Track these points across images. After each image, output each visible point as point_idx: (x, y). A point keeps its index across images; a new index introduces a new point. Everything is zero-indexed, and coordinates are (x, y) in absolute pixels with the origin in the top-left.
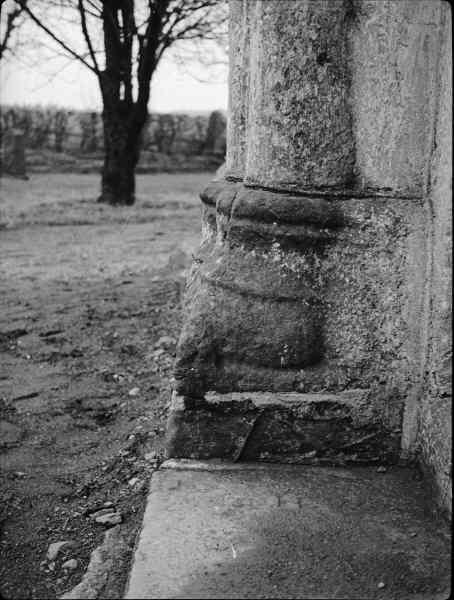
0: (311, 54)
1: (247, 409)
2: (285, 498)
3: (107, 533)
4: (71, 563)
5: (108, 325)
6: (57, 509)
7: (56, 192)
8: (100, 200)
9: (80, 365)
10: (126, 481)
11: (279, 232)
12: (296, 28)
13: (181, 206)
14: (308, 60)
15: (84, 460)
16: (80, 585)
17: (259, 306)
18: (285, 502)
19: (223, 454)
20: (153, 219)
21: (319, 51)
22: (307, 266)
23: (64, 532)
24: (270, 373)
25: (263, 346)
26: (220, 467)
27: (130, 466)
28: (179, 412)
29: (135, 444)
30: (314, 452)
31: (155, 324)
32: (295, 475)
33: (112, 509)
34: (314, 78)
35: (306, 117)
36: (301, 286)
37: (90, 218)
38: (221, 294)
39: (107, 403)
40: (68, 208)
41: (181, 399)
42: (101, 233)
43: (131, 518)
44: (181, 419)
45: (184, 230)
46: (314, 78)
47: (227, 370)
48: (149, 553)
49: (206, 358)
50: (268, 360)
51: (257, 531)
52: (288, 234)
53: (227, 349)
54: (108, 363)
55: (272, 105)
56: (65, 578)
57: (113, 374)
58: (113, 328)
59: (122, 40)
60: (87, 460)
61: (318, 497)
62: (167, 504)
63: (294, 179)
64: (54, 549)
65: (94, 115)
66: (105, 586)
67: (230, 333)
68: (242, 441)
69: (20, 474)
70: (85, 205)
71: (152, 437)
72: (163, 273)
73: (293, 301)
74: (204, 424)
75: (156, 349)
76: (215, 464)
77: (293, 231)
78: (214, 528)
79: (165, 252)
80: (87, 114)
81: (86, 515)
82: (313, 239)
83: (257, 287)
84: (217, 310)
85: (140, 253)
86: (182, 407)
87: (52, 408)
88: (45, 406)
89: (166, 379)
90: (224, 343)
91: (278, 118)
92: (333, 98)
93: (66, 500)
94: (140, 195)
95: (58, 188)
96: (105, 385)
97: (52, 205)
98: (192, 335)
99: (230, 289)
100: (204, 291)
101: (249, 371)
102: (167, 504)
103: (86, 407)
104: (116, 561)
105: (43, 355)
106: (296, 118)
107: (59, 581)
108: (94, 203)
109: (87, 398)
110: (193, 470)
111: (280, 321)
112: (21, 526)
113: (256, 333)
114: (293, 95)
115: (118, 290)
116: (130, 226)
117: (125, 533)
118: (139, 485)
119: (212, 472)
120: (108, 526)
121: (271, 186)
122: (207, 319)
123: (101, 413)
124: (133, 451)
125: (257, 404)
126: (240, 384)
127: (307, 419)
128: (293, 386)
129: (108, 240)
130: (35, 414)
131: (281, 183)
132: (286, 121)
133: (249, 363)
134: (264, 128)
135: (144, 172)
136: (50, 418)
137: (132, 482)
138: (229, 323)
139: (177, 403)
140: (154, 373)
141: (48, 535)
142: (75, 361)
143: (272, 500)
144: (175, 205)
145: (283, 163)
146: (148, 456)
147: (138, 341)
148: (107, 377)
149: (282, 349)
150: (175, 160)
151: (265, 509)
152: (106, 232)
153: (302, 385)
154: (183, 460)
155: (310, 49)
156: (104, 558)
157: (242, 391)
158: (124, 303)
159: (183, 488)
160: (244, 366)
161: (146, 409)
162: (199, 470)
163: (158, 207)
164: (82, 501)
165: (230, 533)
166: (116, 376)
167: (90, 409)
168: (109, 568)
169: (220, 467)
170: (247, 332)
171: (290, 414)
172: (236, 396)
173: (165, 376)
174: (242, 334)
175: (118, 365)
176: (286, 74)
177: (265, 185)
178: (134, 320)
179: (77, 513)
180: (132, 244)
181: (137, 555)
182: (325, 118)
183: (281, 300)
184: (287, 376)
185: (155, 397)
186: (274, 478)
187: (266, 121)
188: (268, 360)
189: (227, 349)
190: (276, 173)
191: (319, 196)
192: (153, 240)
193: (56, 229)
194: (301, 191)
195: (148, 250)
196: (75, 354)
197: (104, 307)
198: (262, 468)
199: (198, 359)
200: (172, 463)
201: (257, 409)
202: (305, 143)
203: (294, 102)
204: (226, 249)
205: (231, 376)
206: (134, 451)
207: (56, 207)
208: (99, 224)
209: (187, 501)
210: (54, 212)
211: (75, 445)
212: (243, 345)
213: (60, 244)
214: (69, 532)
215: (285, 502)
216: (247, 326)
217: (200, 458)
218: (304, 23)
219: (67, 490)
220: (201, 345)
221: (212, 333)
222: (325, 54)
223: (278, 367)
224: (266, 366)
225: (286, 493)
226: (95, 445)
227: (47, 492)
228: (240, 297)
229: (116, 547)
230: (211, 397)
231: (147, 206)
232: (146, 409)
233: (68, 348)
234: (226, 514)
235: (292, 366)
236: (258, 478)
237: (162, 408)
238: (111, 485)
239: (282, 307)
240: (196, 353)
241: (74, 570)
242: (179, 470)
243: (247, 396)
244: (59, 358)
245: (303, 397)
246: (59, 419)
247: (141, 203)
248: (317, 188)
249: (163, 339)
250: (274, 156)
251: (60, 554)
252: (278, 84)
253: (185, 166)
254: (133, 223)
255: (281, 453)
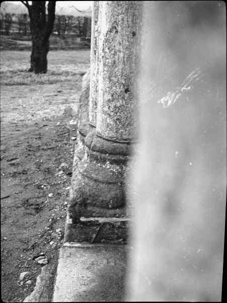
0: (122, 89)
1: (96, 224)
2: (110, 260)
3: (42, 268)
4: (29, 282)
5: (38, 154)
6: (21, 256)
7: (7, 63)
8: (31, 70)
9: (26, 180)
10: (49, 243)
11: (109, 158)
12: (117, 78)
13: (70, 74)
14: (121, 91)
15: (31, 231)
16: (34, 292)
17: (101, 186)
18: (110, 262)
19: (87, 240)
20: (56, 82)
21: (126, 88)
22: (120, 170)
23: (26, 268)
24: (105, 210)
25: (102, 201)
26: (86, 246)
27: (50, 235)
28: (70, 224)
29: (52, 224)
30: (122, 240)
31: (59, 155)
32: (115, 249)
33: (44, 257)
34: (123, 98)
35: (120, 113)
36: (118, 177)
37: (26, 81)
38: (86, 180)
39: (40, 201)
40: (14, 74)
41: (71, 220)
42: (32, 90)
43: (53, 261)
44: (71, 227)
45: (71, 89)
46: (123, 98)
47: (88, 209)
48: (60, 287)
49: (81, 205)
50: (105, 206)
51: (99, 276)
52: (113, 159)
53: (89, 201)
54: (39, 178)
55: (107, 107)
56: (27, 288)
57: (41, 185)
58: (41, 156)
59: (41, 14)
60: (32, 232)
61: (122, 260)
62: (66, 264)
63: (115, 136)
64: (22, 275)
65: (25, 15)
66: (42, 293)
67: (90, 195)
68: (94, 236)
69: (6, 238)
70: (23, 73)
71: (59, 220)
72: (62, 119)
73: (114, 183)
74: (80, 229)
75: (59, 170)
76: (85, 244)
77: (114, 158)
78: (83, 275)
79: (63, 103)
80: (21, 15)
81: (34, 259)
82: (122, 160)
83: (100, 178)
84: (85, 186)
85: (50, 103)
86: (71, 222)
87: (16, 205)
88: (13, 203)
89: (64, 188)
90: (88, 199)
91: (109, 112)
92: (131, 105)
93: (25, 251)
94: (50, 67)
95: (8, 60)
96: (38, 191)
97: (6, 72)
98: (75, 196)
99: (91, 178)
100: (80, 177)
101: (97, 210)
102: (66, 264)
103: (31, 203)
104: (46, 281)
105: (10, 174)
106: (116, 113)
107: (25, 290)
108: (27, 72)
109: (30, 198)
110: (76, 247)
111: (109, 192)
112: (8, 264)
113: (100, 196)
114: (115, 104)
115: (41, 131)
116: (45, 86)
117: (49, 268)
118: (54, 246)
119: (83, 248)
120: (43, 265)
121: (106, 138)
122: (81, 190)
123: (37, 207)
124: (51, 228)
125: (100, 222)
126: (94, 214)
127: (119, 227)
128: (114, 216)
129: (36, 96)
130: (9, 207)
131: (110, 137)
132: (112, 114)
133: (98, 207)
134: (103, 115)
135: (52, 49)
136: (16, 209)
137: (51, 243)
138: (90, 192)
139: (69, 221)
140: (59, 184)
141: (19, 269)
142: (24, 177)
143: (105, 261)
144: (67, 73)
145: (111, 130)
146: (58, 231)
147: (51, 165)
148: (39, 187)
149: (110, 202)
150: (66, 42)
151: (102, 266)
152: (34, 90)
153: (117, 215)
154: (72, 242)
155: (122, 87)
156: (42, 280)
157: (95, 217)
158: (44, 140)
159: (72, 256)
160: (95, 208)
161: (56, 205)
162: (79, 247)
163: (59, 74)
164: (31, 252)
165: (89, 277)
166: (42, 186)
167: (32, 205)
168: (43, 284)
169: (86, 246)
170: (96, 196)
171: (112, 226)
172: (92, 219)
173: (64, 186)
174: (94, 197)
175: (43, 179)
176: (112, 96)
177: (104, 137)
178: (49, 152)
179: (30, 258)
180: (47, 98)
181: (55, 288)
182: (128, 113)
183: (110, 183)
184: (112, 212)
185: (59, 198)
186: (106, 251)
187: (104, 112)
188: (105, 206)
189: (89, 201)
190: (108, 133)
191: (124, 143)
192: (56, 95)
193: (9, 87)
194: (118, 141)
195: (54, 102)
196: (24, 172)
197: (36, 143)
198: (102, 245)
199: (77, 205)
200: (67, 244)
201: (100, 224)
202: (120, 122)
203: (115, 107)
204: (88, 161)
205: (91, 211)
206: (52, 228)
207: (9, 74)
208: (30, 85)
209: (73, 262)
210: (8, 77)
211: (27, 223)
212: (94, 201)
213: (12, 98)
214: (28, 267)
215: (110, 262)
216: (96, 193)
217: (79, 242)
218: (120, 77)
219: (25, 247)
220: (79, 200)
221: (83, 196)
222: (128, 89)
223: (108, 208)
224: (104, 208)
225: (110, 258)
226: (35, 223)
227: (17, 247)
228: (94, 182)
229: (47, 275)
230: (83, 219)
231: (53, 74)
232: (56, 205)
233: (20, 169)
234: (87, 268)
235: (114, 208)
236: (100, 251)
237: (63, 204)
238: (43, 244)
239: (110, 186)
240: (77, 203)
241: (30, 285)
242: (70, 247)
243: (96, 219)
244: (17, 174)
245: (118, 219)
246: (19, 209)
247: (51, 72)
248: (124, 140)
249: (63, 165)
250: (108, 126)
251: (25, 278)
252: (109, 99)
253: (71, 46)
254: (46, 84)
255: (109, 239)
